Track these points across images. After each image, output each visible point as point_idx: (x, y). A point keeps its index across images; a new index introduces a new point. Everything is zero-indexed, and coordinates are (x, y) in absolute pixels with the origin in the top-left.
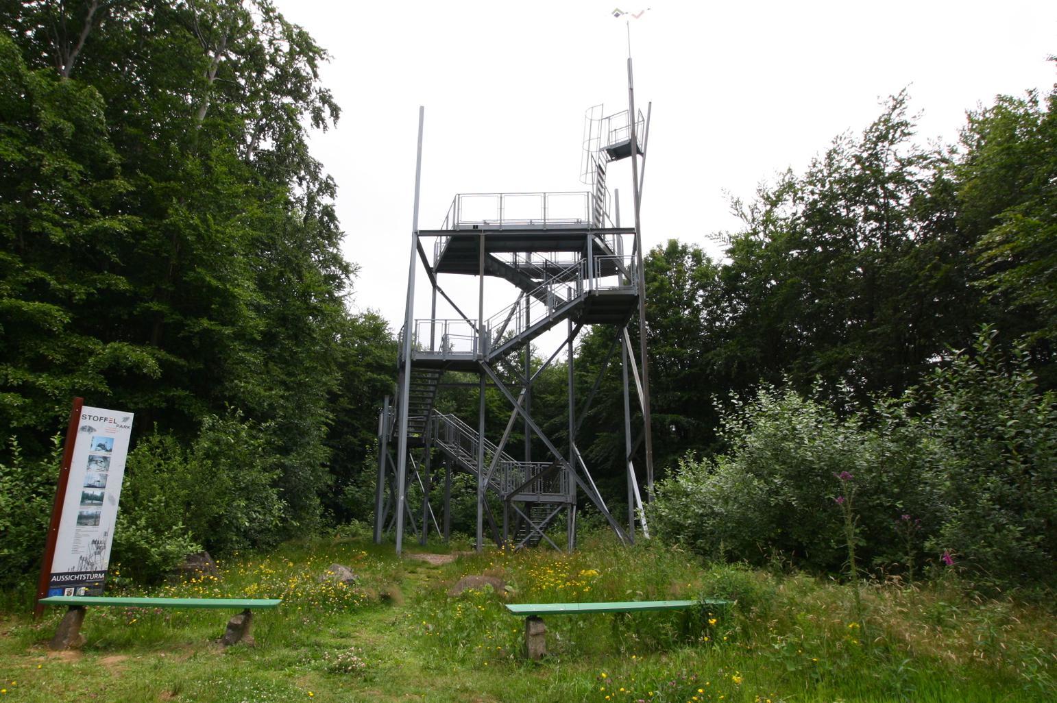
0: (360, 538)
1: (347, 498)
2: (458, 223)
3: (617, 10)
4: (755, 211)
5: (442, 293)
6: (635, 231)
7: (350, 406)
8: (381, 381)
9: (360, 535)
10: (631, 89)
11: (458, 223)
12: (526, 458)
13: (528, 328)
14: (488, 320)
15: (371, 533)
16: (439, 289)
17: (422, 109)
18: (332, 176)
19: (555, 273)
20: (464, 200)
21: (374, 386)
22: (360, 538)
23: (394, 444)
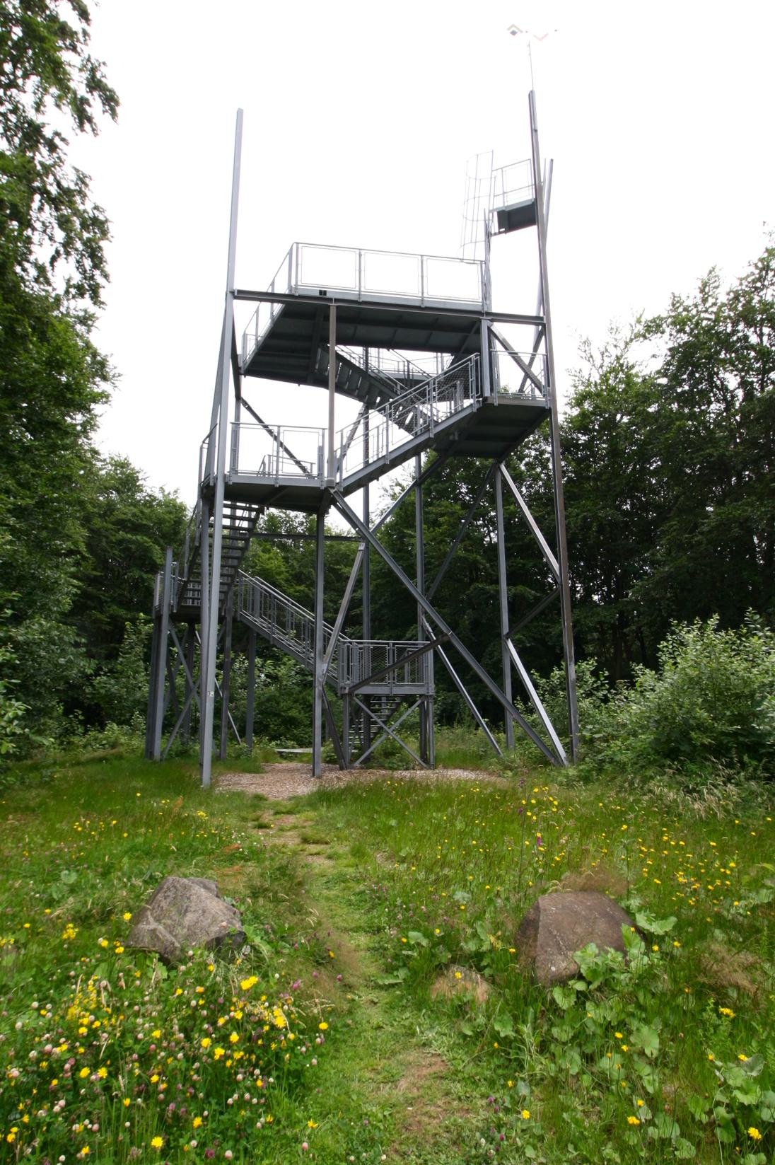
0: (122, 749)
1: (99, 693)
2: (296, 285)
3: (513, 26)
4: (606, 354)
5: (249, 409)
6: (541, 324)
7: (95, 573)
8: (136, 542)
9: (122, 744)
10: (534, 131)
11: (296, 285)
12: (365, 636)
13: (367, 464)
14: (342, 431)
15: (138, 743)
16: (245, 403)
17: (240, 114)
18: (98, 204)
19: (414, 388)
20: (305, 253)
21: (129, 549)
22: (122, 749)
23: (189, 616)
